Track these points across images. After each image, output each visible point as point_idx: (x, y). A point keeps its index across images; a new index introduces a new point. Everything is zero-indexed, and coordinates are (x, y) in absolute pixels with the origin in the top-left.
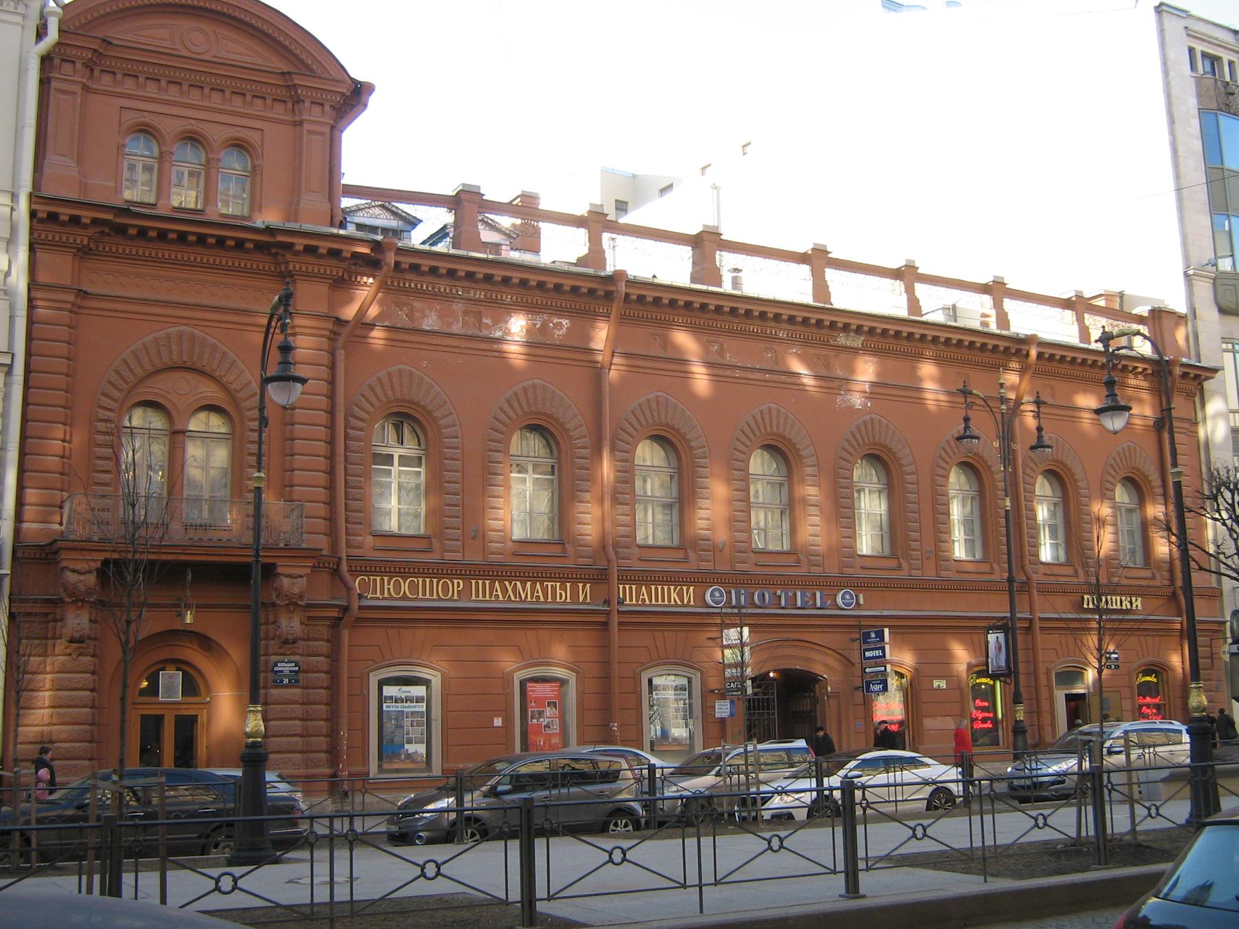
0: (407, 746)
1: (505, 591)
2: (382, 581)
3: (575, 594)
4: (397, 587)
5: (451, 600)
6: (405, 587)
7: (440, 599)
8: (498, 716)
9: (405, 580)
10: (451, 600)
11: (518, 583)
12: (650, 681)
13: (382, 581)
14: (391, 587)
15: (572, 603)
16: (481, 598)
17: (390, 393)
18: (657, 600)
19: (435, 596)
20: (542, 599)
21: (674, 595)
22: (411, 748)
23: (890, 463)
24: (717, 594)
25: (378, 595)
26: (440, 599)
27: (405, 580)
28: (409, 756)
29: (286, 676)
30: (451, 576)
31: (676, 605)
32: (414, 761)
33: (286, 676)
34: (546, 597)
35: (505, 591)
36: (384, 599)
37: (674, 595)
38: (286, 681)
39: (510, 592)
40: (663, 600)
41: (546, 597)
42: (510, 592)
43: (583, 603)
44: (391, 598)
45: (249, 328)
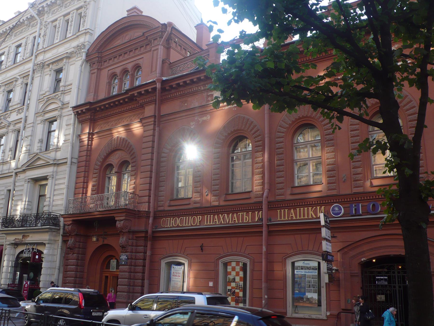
0: (307, 294)
1: (219, 219)
2: (308, 209)
3: (253, 218)
4: (176, 221)
5: (196, 225)
6: (178, 221)
7: (192, 226)
8: (211, 281)
9: (178, 218)
10: (196, 225)
11: (226, 215)
12: (293, 263)
13: (308, 209)
14: (173, 222)
15: (253, 222)
16: (287, 219)
17: (243, 126)
18: (300, 216)
19: (190, 225)
20: (237, 222)
21: (311, 212)
22: (309, 295)
23: (242, 134)
24: (337, 209)
25: (169, 226)
26: (192, 226)
27: (178, 218)
28: (308, 299)
29: (123, 261)
30: (197, 215)
31: (313, 218)
32: (311, 303)
33: (123, 261)
34: (238, 220)
35: (219, 219)
36: (170, 227)
37: (311, 212)
38: (123, 263)
39: (221, 218)
40: (304, 216)
41: (238, 220)
42: (222, 220)
43: (228, 223)
44: (173, 227)
45: (174, 120)
